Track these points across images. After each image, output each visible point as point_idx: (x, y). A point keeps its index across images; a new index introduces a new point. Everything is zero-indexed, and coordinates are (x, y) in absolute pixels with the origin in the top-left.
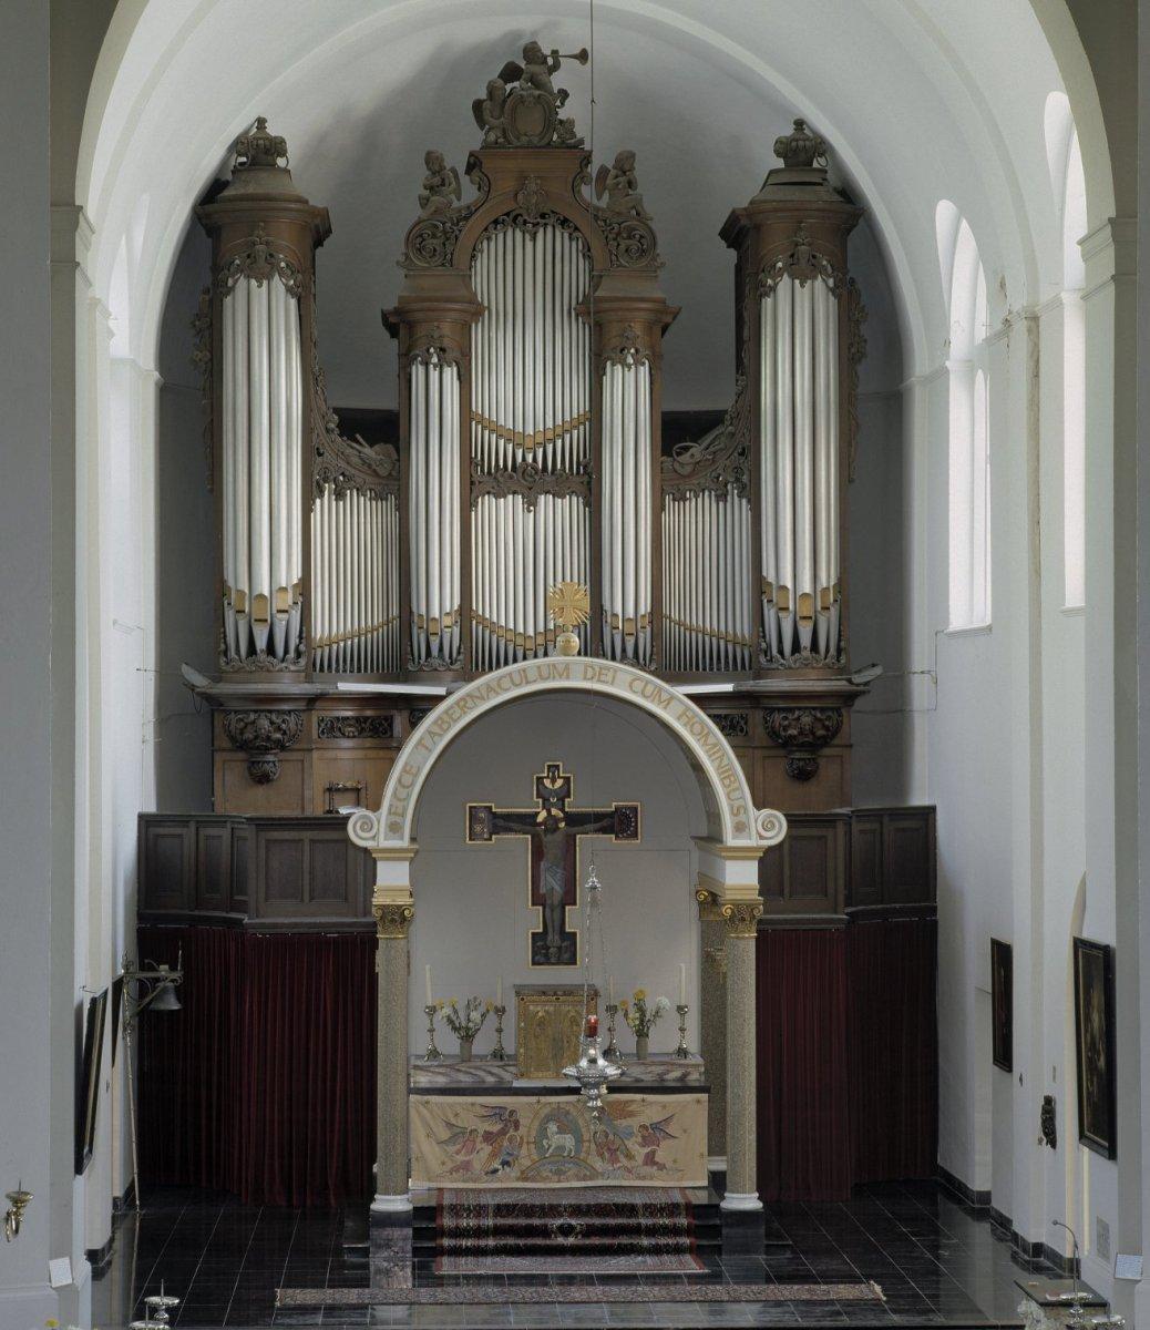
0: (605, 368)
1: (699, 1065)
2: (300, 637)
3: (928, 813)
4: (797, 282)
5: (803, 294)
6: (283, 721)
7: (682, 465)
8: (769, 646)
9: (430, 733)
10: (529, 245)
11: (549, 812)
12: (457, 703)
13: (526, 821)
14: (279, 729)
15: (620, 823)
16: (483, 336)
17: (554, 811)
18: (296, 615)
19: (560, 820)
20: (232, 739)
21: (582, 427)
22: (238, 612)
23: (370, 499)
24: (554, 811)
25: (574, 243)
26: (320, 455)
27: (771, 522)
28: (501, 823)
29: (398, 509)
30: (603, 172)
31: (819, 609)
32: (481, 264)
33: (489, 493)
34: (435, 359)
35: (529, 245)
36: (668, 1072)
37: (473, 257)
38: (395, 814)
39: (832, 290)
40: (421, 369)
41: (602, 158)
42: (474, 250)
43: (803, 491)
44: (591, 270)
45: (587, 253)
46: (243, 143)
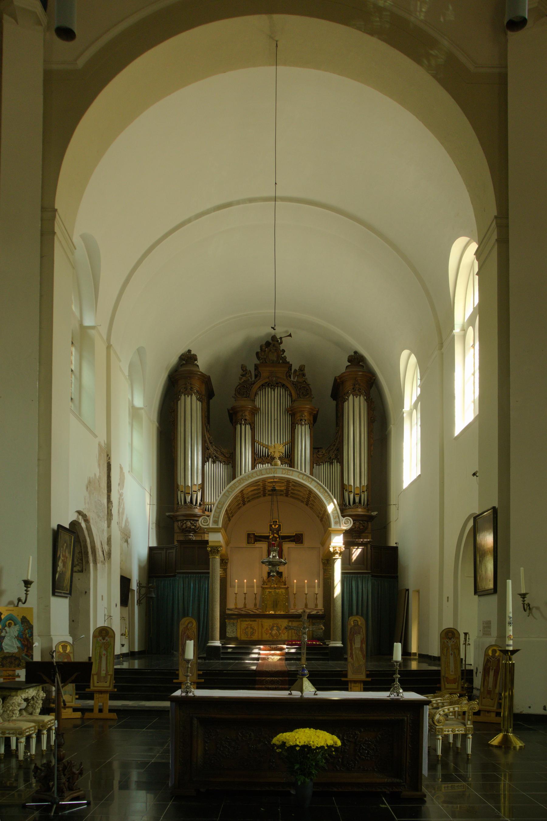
0: (295, 427)
1: (322, 610)
2: (201, 500)
3: (395, 549)
4: (355, 397)
5: (357, 400)
6: (195, 523)
7: (319, 455)
8: (346, 504)
9: (228, 491)
10: (273, 392)
11: (274, 535)
12: (237, 481)
13: (266, 538)
14: (194, 525)
15: (298, 539)
16: (258, 418)
17: (275, 535)
18: (199, 494)
19: (277, 538)
20: (179, 528)
21: (288, 444)
22: (181, 492)
23: (224, 465)
24: (275, 535)
25: (286, 392)
26: (208, 449)
27: (346, 423)
28: (258, 538)
29: (232, 467)
30: (295, 371)
31: (361, 491)
32: (257, 399)
33: (260, 463)
34: (243, 422)
35: (273, 392)
36: (312, 612)
37: (255, 395)
38: (215, 517)
39: (366, 400)
40: (239, 426)
41: (295, 366)
42: (256, 393)
43: (357, 466)
44: (292, 399)
45: (291, 395)
46: (183, 355)
